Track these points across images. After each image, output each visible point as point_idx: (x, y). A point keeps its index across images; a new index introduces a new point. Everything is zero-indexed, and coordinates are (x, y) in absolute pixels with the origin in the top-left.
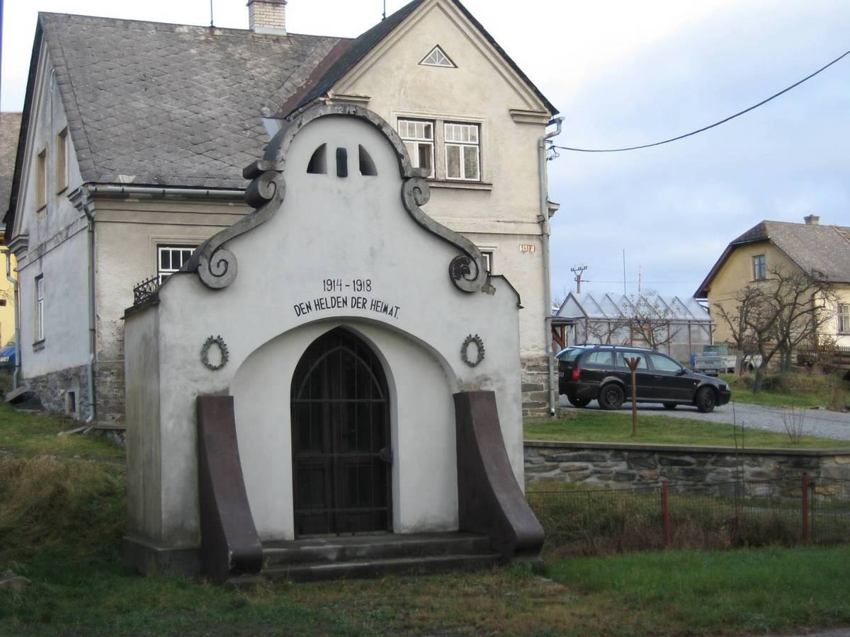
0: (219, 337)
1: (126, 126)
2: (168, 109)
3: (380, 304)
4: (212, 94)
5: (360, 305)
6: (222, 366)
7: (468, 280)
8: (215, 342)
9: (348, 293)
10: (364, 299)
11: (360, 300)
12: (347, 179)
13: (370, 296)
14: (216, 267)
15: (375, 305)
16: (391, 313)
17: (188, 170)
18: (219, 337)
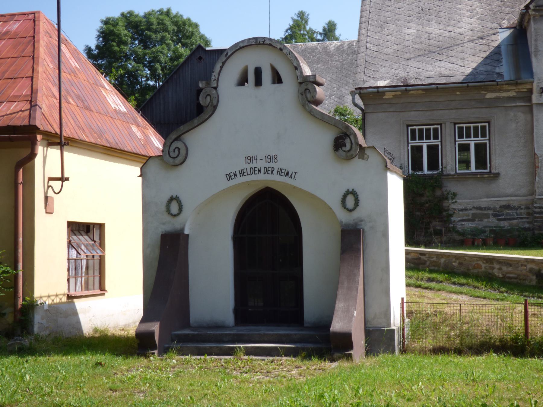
0: (177, 196)
1: (395, 47)
2: (430, 31)
3: (283, 171)
4: (467, 17)
5: (270, 172)
6: (178, 214)
7: (344, 151)
8: (175, 199)
9: (262, 164)
10: (272, 168)
11: (270, 169)
12: (261, 87)
13: (276, 166)
14: (173, 152)
15: (280, 172)
16: (291, 177)
17: (429, 72)
18: (177, 196)
